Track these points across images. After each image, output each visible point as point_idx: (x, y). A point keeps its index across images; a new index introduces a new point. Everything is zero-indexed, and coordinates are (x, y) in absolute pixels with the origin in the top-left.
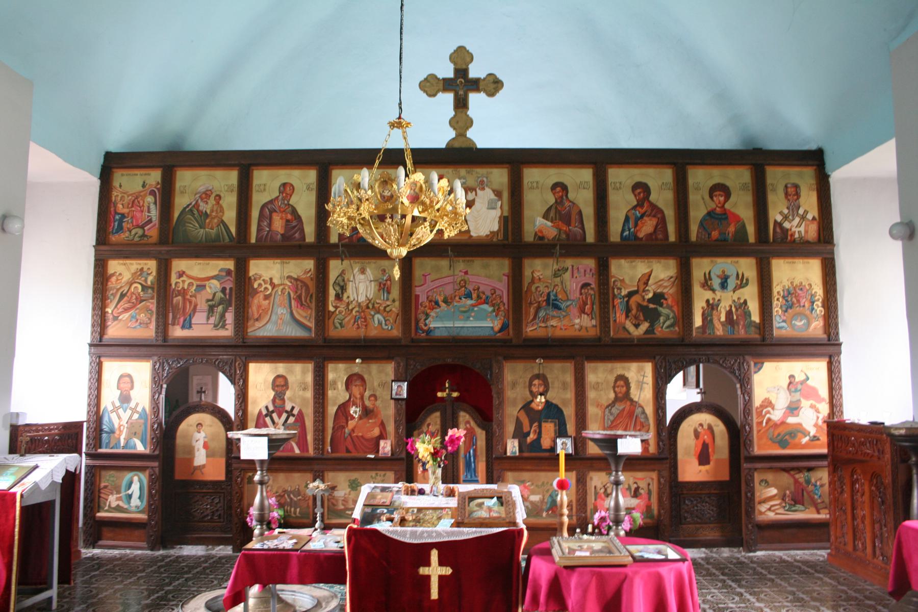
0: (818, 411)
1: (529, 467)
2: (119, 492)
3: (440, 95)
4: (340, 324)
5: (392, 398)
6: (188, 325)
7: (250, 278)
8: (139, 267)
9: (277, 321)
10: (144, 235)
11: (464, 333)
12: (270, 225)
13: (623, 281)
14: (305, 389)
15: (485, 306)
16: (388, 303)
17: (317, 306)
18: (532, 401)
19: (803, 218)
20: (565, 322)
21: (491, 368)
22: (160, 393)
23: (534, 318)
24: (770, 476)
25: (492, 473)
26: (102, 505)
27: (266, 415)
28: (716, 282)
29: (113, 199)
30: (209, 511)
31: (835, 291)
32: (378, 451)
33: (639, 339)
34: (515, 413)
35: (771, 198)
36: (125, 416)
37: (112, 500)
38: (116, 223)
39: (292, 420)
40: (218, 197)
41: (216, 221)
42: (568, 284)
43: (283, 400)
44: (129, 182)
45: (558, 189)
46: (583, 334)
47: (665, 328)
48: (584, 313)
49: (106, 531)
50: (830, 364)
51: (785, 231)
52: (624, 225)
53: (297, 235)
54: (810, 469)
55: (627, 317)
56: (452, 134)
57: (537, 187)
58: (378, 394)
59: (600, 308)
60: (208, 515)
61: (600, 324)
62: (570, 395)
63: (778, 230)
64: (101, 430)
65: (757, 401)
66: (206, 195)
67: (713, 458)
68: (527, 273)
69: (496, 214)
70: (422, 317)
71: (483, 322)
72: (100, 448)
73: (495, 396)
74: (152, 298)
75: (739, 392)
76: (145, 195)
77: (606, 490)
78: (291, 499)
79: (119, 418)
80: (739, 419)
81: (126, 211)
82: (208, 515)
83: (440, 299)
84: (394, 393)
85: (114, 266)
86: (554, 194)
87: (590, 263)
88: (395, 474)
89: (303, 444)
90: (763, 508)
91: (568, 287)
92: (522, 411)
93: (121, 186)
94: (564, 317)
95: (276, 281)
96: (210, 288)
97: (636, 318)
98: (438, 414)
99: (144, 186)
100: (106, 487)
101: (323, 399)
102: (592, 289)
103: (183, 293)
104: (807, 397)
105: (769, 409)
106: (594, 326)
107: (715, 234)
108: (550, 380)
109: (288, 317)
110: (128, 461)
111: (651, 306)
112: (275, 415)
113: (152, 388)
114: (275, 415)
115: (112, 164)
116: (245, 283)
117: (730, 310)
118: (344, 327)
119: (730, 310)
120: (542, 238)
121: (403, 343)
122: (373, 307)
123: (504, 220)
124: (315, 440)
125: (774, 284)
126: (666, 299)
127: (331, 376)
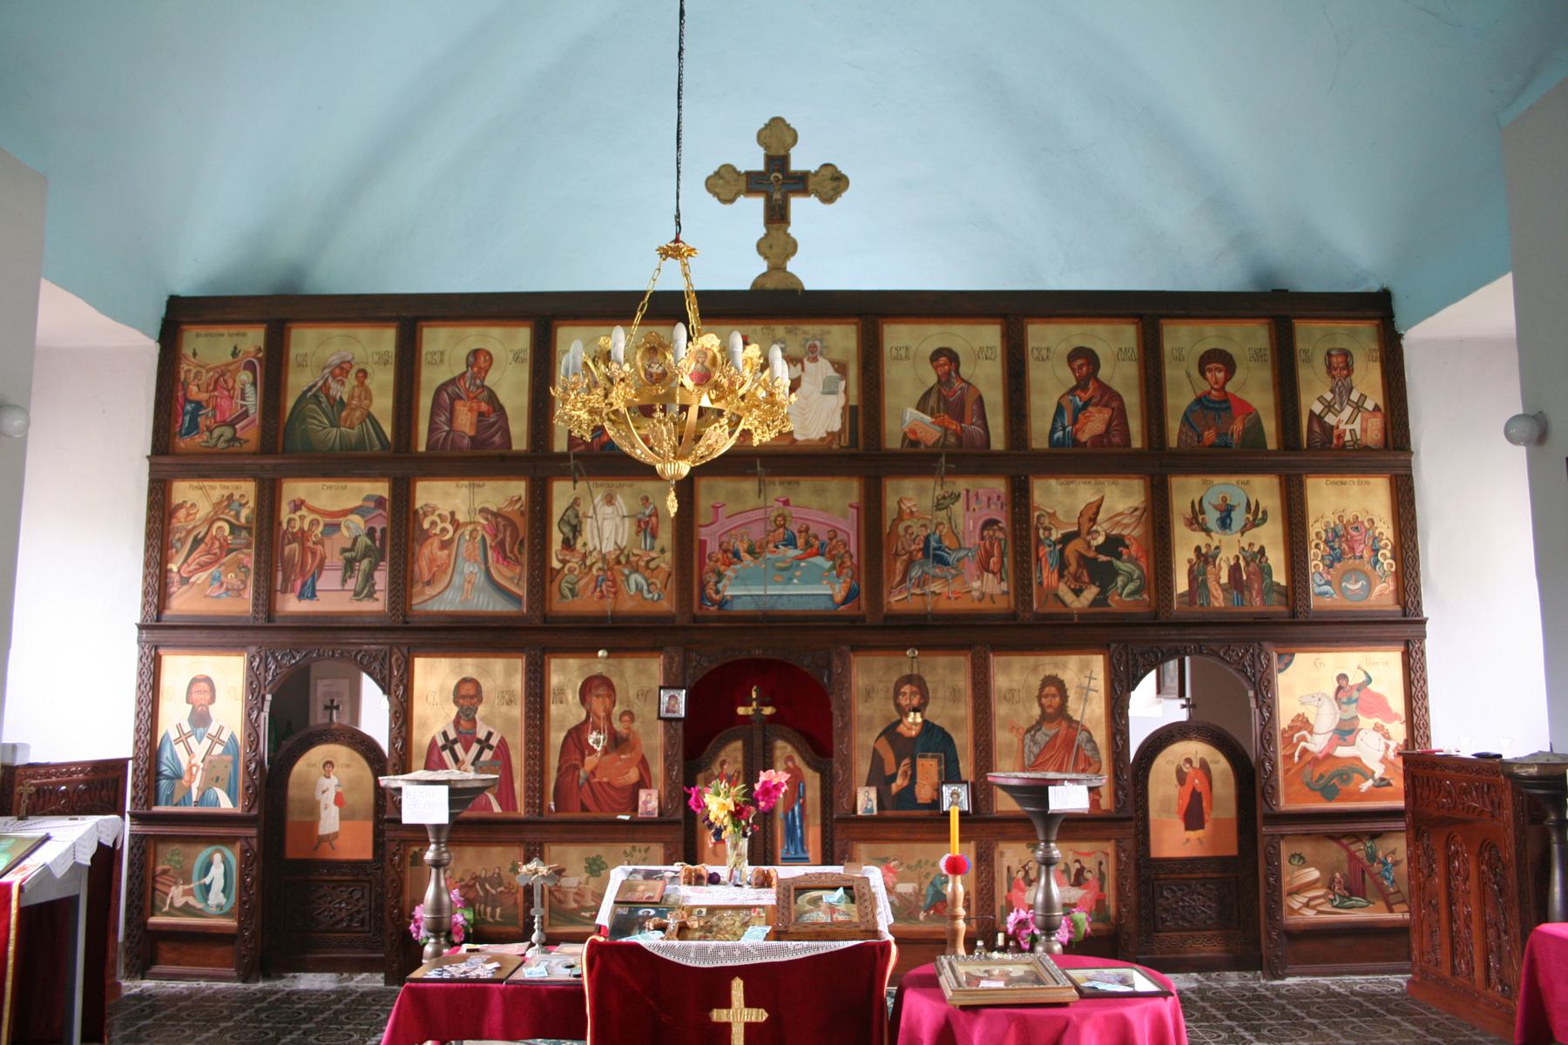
0: (1387, 736)
1: (894, 835)
2: (187, 881)
3: (741, 199)
4: (571, 590)
5: (660, 718)
6: (309, 592)
7: (416, 512)
8: (227, 493)
9: (462, 585)
10: (234, 439)
11: (783, 606)
12: (451, 421)
13: (1053, 515)
14: (510, 702)
15: (819, 560)
16: (653, 554)
17: (531, 560)
18: (900, 721)
19: (1358, 407)
20: (955, 586)
21: (829, 665)
22: (261, 710)
23: (903, 580)
24: (1306, 848)
25: (832, 846)
26: (158, 902)
27: (444, 748)
28: (1212, 517)
29: (182, 376)
30: (343, 914)
31: (1414, 531)
32: (636, 809)
33: (1082, 615)
34: (871, 742)
35: (1303, 373)
36: (200, 749)
37: (177, 895)
38: (187, 418)
39: (487, 755)
40: (363, 374)
41: (358, 414)
42: (960, 521)
43: (473, 721)
44: (209, 348)
45: (943, 360)
46: (986, 606)
47: (1125, 596)
48: (988, 571)
49: (164, 949)
50: (1407, 656)
51: (1328, 430)
52: (1055, 421)
53: (497, 438)
54: (1374, 836)
55: (1061, 576)
56: (761, 266)
57: (907, 357)
58: (635, 710)
59: (1015, 563)
60: (342, 920)
61: (1015, 589)
62: (964, 711)
63: (1316, 428)
64: (159, 773)
65: (1284, 720)
66: (342, 369)
67: (1210, 817)
68: (891, 502)
69: (836, 402)
70: (712, 578)
71: (815, 587)
72: (156, 804)
73: (836, 712)
74: (248, 546)
75: (1253, 704)
76: (237, 370)
77: (1027, 873)
78: (486, 891)
79: (190, 752)
80: (1253, 751)
81: (203, 396)
82: (342, 920)
83: (742, 547)
84: (663, 707)
85: (183, 491)
86: (936, 368)
87: (998, 485)
88: (666, 849)
89: (506, 797)
90: (1296, 902)
91: (961, 528)
92: (883, 739)
93: (195, 354)
94: (954, 577)
95: (461, 517)
96: (348, 528)
97: (1076, 578)
98: (739, 744)
99: (235, 354)
100: (165, 872)
101: (542, 718)
102: (1001, 529)
103: (302, 536)
104: (1369, 713)
105: (1304, 732)
106: (1004, 593)
107: (1209, 435)
108: (929, 686)
109: (481, 578)
110: (204, 827)
111: (1102, 558)
112: (458, 748)
113: (247, 702)
114: (458, 748)
115: (181, 316)
116: (407, 519)
117: (1237, 564)
118: (577, 597)
119: (1237, 564)
120: (915, 443)
121: (679, 622)
122: (628, 561)
123: (850, 413)
124: (527, 789)
125: (1311, 520)
126: (1127, 547)
127: (555, 680)
